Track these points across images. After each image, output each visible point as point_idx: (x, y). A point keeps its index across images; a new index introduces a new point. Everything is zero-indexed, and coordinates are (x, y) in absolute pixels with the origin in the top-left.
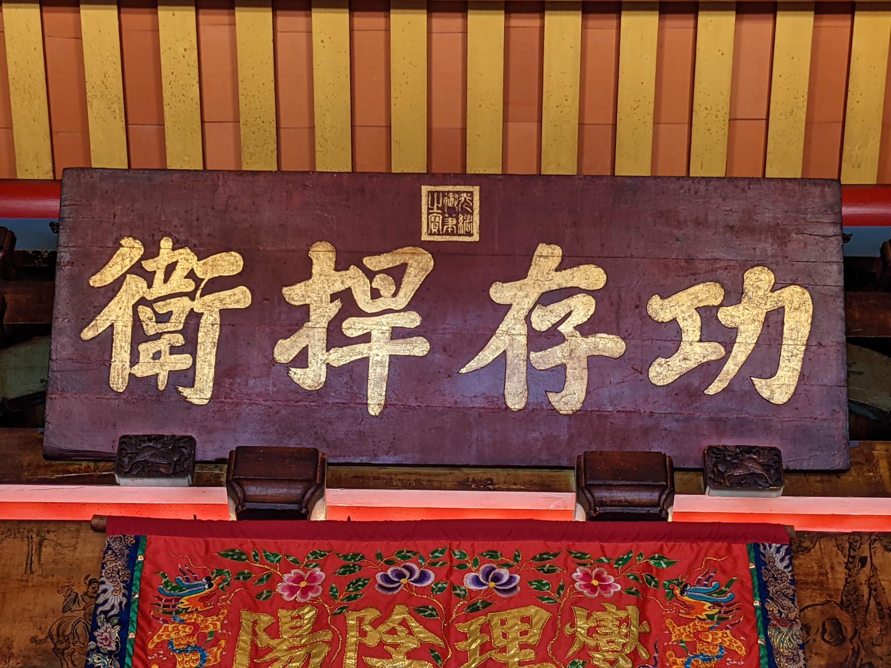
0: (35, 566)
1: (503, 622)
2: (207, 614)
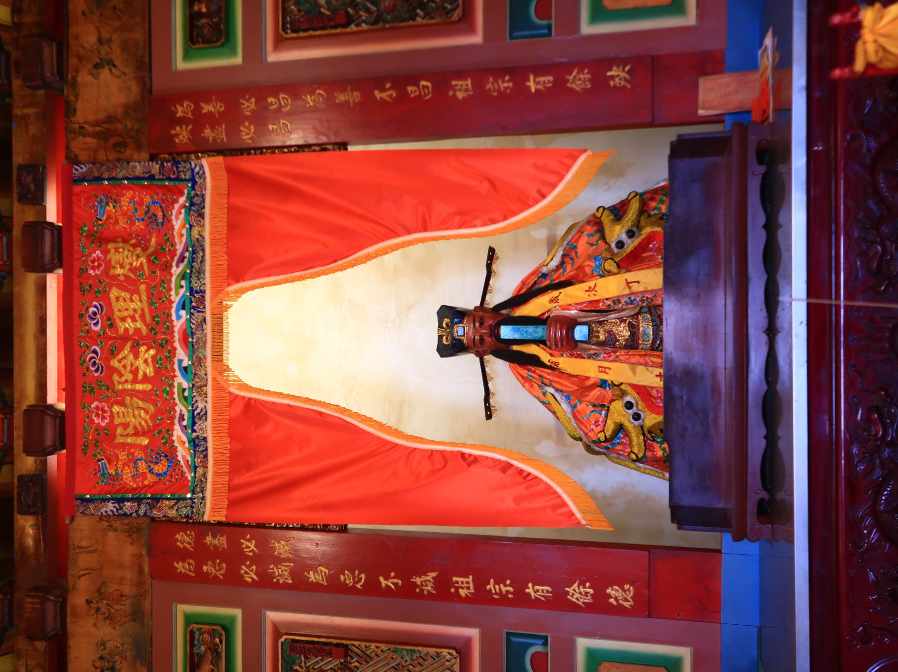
1: (120, 310)
2: (118, 459)
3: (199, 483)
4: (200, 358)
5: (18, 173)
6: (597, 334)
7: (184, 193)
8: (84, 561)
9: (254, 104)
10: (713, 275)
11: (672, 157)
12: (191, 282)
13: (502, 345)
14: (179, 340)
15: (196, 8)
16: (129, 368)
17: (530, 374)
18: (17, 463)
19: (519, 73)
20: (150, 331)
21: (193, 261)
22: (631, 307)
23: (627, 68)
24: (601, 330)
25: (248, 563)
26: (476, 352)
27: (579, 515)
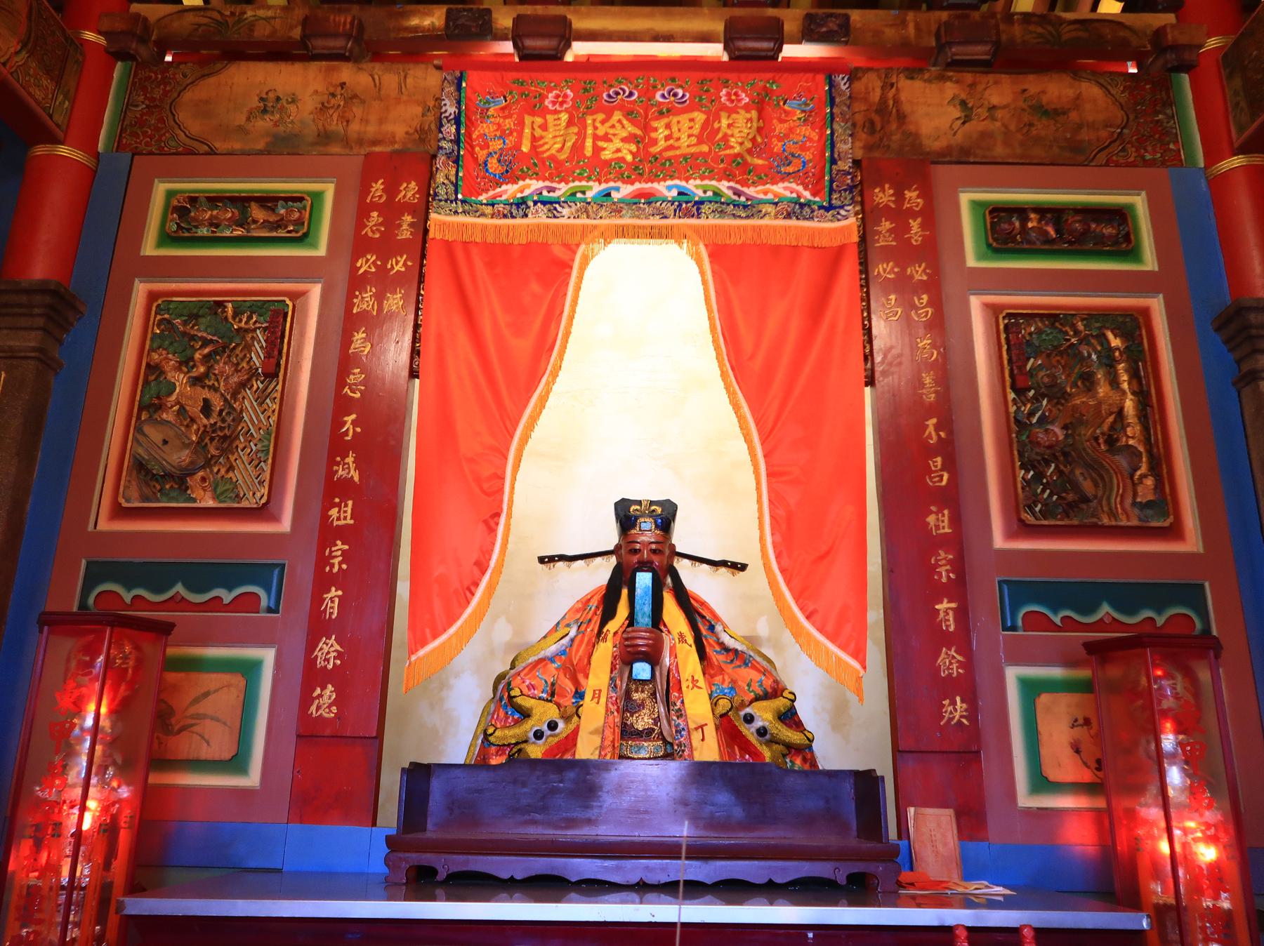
0: (403, 90)
1: (678, 122)
2: (505, 118)
3: (475, 209)
4: (621, 211)
5: (840, 14)
6: (640, 689)
7: (815, 197)
8: (389, 78)
9: (920, 278)
10: (713, 824)
11: (856, 774)
12: (710, 202)
13: (629, 576)
14: (643, 188)
15: (1032, 216)
16: (611, 131)
17: (593, 608)
18: (505, 9)
19: (959, 589)
20: (654, 156)
21: (734, 206)
22: (672, 731)
23: (964, 721)
24: (644, 695)
25: (379, 263)
26: (621, 546)
27: (421, 653)
